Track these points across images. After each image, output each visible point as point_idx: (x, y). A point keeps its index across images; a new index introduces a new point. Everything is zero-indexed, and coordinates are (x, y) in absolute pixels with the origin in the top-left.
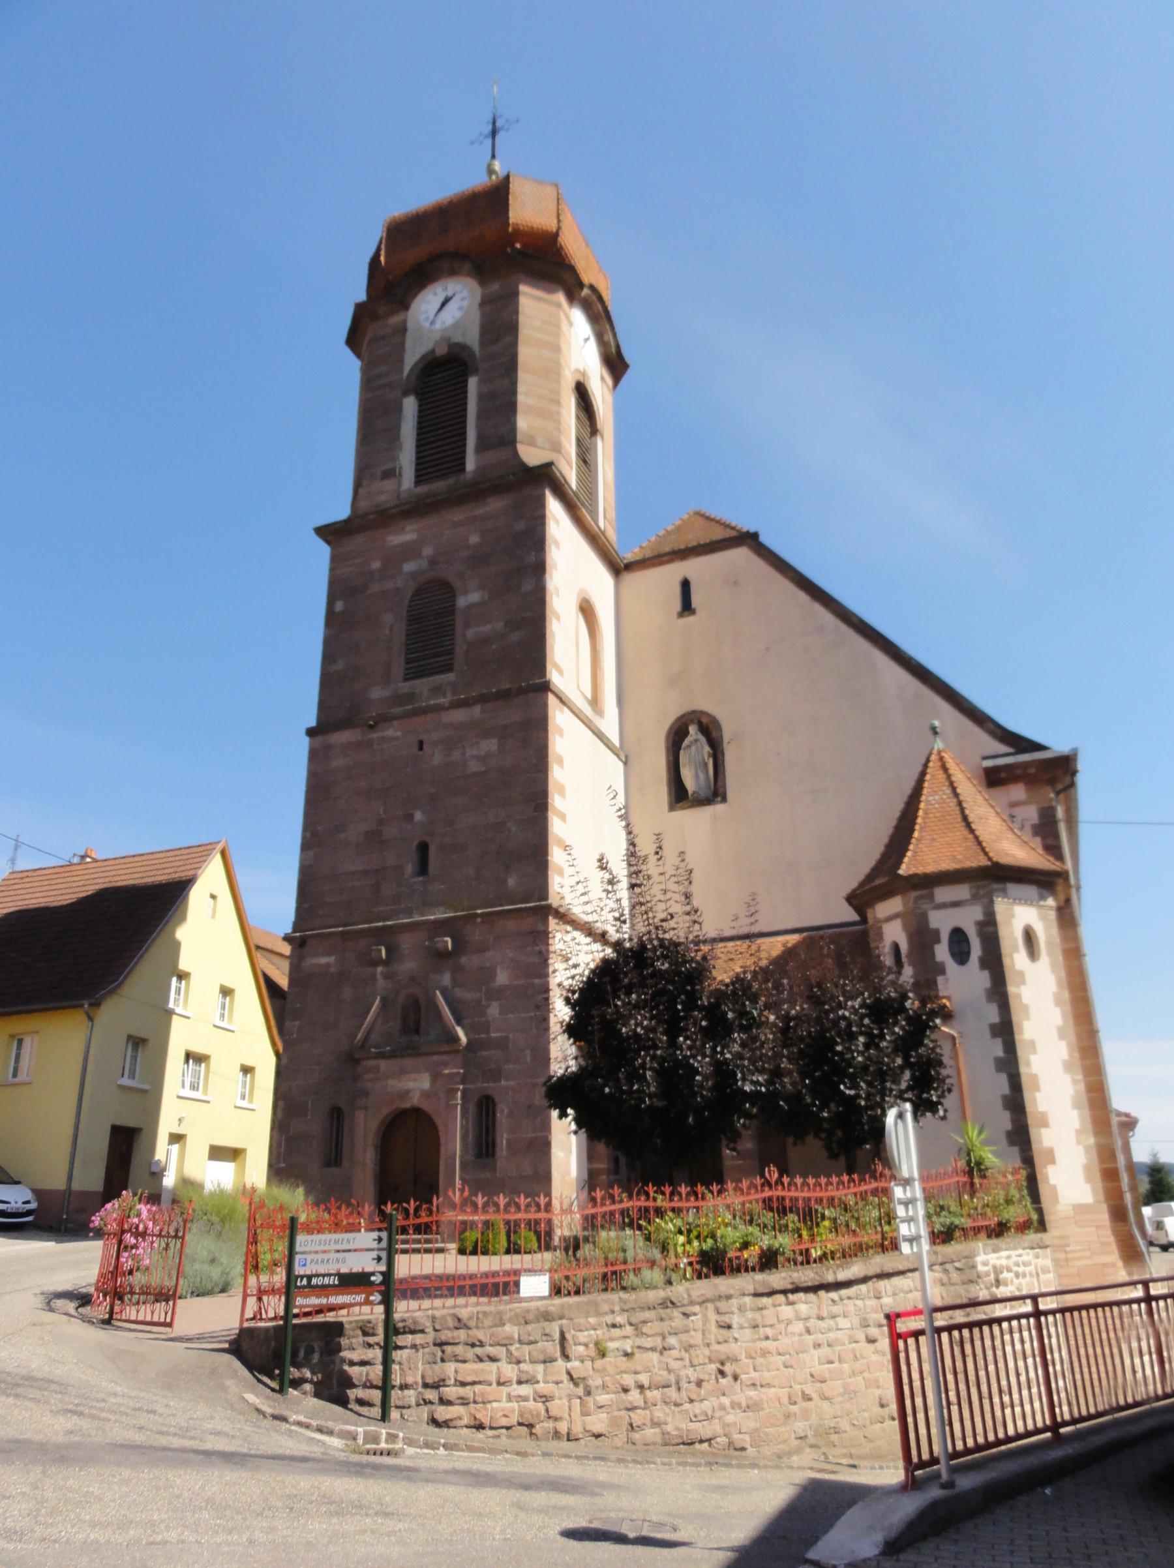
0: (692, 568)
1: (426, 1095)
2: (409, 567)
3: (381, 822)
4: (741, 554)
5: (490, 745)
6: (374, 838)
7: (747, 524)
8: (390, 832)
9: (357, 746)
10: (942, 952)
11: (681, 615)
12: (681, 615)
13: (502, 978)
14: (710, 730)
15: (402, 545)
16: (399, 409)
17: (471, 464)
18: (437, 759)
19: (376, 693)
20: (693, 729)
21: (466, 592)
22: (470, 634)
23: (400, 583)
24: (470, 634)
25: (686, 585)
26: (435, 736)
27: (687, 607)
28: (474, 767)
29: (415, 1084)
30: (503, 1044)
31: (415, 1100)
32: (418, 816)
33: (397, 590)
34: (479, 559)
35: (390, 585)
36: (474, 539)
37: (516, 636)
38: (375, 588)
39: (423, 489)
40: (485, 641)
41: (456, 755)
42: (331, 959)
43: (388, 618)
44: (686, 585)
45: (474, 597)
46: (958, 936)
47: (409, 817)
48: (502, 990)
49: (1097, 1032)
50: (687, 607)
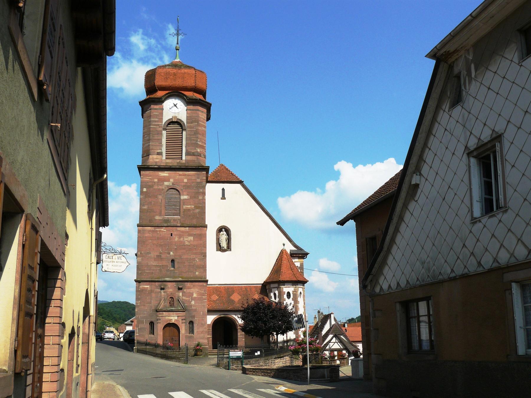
0: (226, 186)
1: (176, 320)
2: (166, 183)
3: (161, 253)
4: (239, 185)
5: (191, 238)
6: (159, 258)
7: (241, 179)
8: (163, 256)
9: (153, 231)
10: (285, 296)
11: (222, 199)
12: (222, 199)
13: (195, 295)
14: (228, 231)
15: (164, 176)
16: (161, 134)
17: (184, 158)
18: (176, 239)
19: (157, 218)
20: (223, 230)
21: (183, 195)
22: (185, 207)
23: (163, 188)
24: (185, 207)
25: (223, 190)
26: (175, 233)
27: (223, 197)
28: (187, 243)
29: (173, 318)
30: (195, 310)
31: (173, 322)
32: (172, 253)
33: (163, 189)
34: (187, 187)
35: (160, 187)
36: (185, 180)
37: (197, 211)
38: (156, 187)
39: (168, 161)
40: (189, 210)
41: (182, 239)
42: (148, 286)
43: (160, 197)
44: (223, 190)
45: (186, 197)
46: (289, 294)
47: (169, 253)
48: (195, 298)
49: (114, 301)
50: (223, 197)
